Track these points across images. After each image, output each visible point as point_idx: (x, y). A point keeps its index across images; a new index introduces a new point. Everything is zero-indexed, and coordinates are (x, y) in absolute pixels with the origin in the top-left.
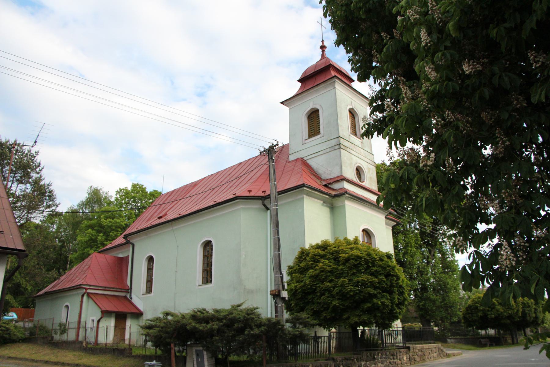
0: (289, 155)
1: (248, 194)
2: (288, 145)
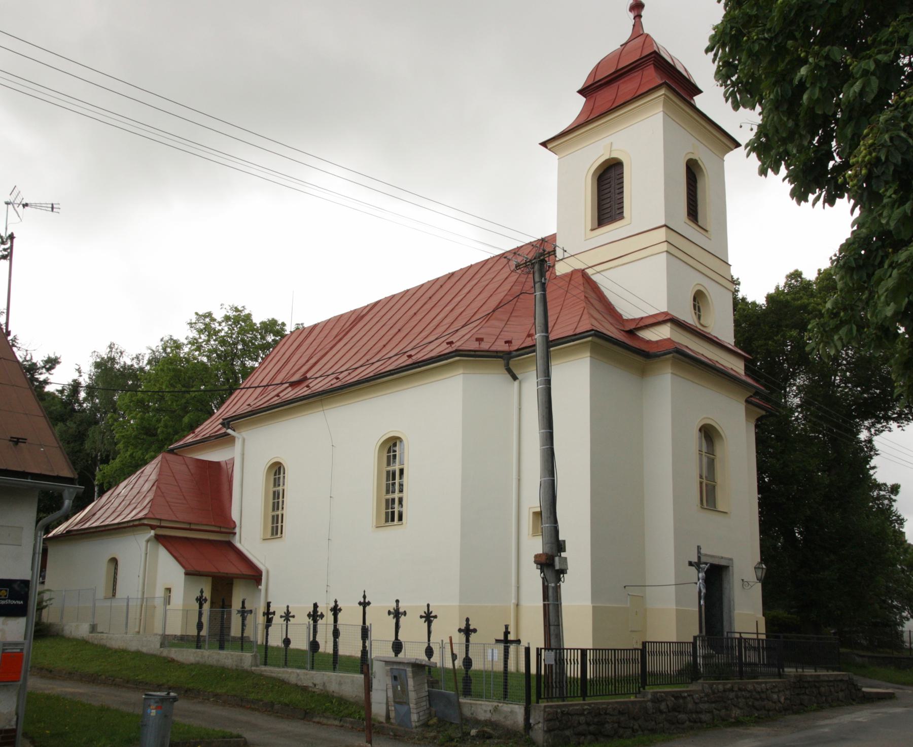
1: (474, 346)
2: (554, 237)
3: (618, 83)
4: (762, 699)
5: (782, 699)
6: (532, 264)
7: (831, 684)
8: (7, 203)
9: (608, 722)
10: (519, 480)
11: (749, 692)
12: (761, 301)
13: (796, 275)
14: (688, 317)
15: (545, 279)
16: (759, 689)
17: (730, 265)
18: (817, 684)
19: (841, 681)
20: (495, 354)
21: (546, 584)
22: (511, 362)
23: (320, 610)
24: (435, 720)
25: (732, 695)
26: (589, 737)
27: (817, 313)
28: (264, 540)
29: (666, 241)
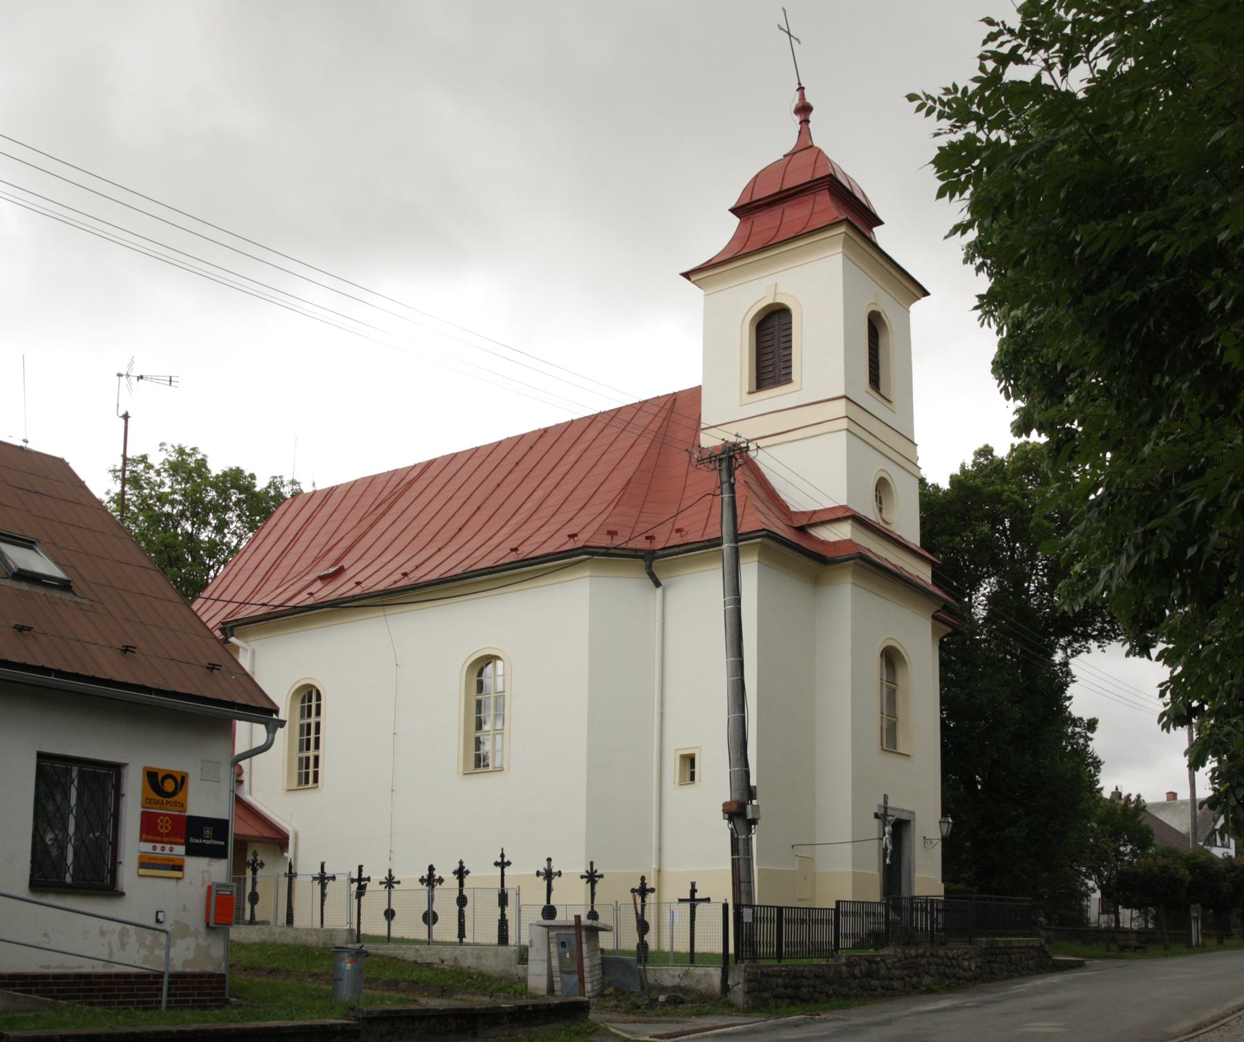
0: (697, 428)
1: (604, 541)
2: (694, 395)
3: (784, 205)
4: (953, 966)
5: (973, 967)
6: (720, 460)
7: (1023, 950)
8: (119, 375)
9: (805, 986)
10: (662, 714)
11: (940, 958)
12: (945, 485)
13: (986, 451)
14: (870, 513)
15: (735, 479)
16: (950, 956)
17: (916, 445)
18: (1008, 950)
19: (1033, 947)
20: (633, 553)
21: (736, 836)
22: (654, 564)
23: (437, 874)
24: (611, 990)
25: (924, 961)
26: (787, 1000)
27: (1012, 503)
28: (288, 790)
29: (846, 417)
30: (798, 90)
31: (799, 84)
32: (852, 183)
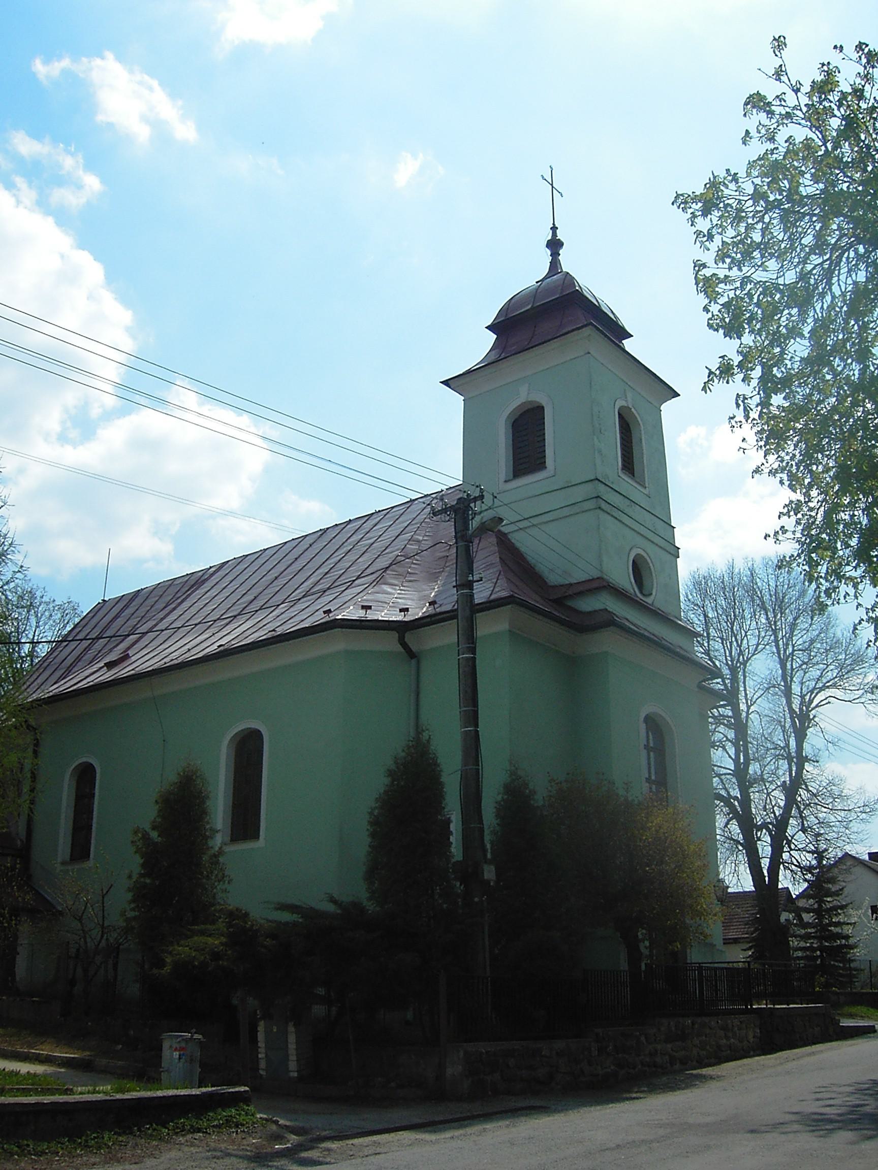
30: (551, 228)
31: (554, 224)
32: (599, 301)
